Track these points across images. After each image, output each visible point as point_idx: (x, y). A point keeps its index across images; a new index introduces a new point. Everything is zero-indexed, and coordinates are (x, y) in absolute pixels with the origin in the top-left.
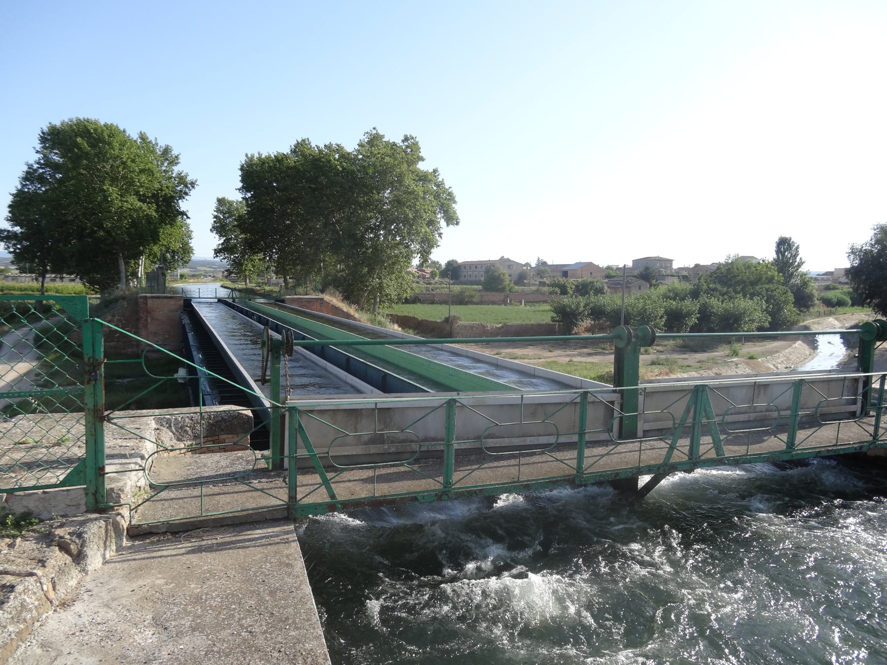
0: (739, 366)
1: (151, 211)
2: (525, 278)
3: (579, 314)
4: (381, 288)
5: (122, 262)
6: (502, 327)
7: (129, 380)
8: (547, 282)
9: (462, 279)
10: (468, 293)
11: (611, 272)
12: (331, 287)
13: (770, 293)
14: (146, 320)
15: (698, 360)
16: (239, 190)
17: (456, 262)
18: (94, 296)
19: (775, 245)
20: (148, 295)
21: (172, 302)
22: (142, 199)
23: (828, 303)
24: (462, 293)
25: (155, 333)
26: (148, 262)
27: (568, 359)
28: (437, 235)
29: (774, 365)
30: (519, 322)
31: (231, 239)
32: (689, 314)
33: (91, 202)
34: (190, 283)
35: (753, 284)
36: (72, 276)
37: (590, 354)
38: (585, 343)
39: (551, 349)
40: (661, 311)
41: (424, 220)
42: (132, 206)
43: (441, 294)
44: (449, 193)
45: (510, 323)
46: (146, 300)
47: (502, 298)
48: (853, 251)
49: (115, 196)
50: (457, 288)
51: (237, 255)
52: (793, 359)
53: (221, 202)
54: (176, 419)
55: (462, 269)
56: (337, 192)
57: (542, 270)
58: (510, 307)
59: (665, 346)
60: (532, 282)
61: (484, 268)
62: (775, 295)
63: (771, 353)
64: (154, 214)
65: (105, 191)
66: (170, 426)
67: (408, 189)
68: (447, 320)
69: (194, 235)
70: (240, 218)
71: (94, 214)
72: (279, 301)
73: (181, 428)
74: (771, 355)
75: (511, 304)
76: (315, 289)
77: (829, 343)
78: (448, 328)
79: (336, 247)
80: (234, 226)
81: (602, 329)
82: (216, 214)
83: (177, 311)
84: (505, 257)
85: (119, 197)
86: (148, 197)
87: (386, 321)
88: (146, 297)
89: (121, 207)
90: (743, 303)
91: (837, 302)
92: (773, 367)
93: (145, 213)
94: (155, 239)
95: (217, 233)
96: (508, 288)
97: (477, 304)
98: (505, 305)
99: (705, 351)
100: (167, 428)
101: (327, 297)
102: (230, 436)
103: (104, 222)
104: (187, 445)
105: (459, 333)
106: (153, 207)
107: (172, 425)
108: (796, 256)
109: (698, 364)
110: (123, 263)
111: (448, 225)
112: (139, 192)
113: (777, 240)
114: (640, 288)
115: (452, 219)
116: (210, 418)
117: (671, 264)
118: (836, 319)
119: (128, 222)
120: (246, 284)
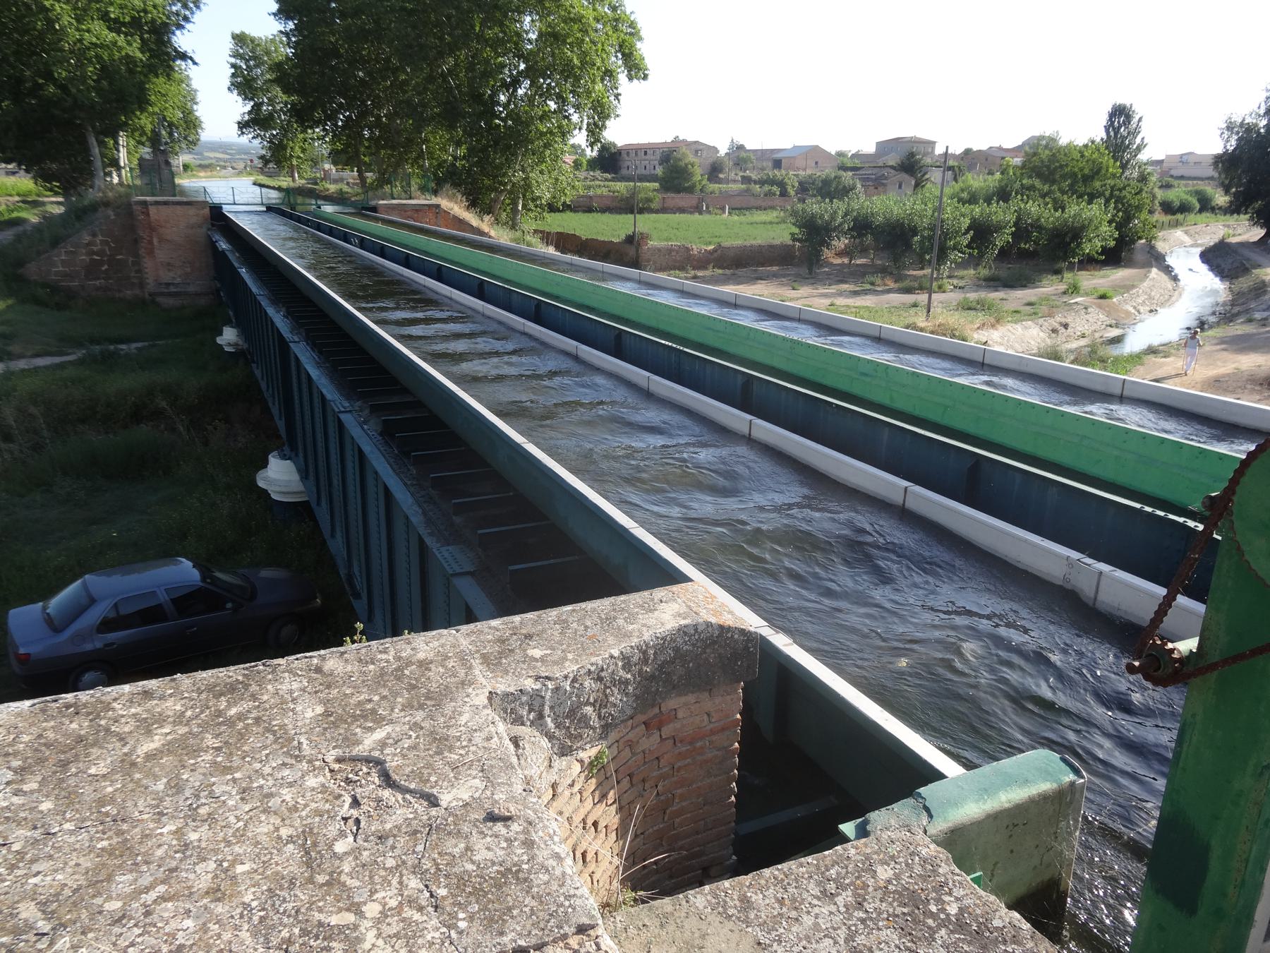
0: (1089, 310)
1: (133, 49)
2: (721, 171)
3: (835, 229)
4: (527, 186)
5: (92, 141)
6: (715, 251)
7: (139, 345)
8: (754, 177)
9: (624, 172)
10: (642, 195)
11: (845, 160)
12: (448, 186)
13: (1117, 193)
14: (151, 242)
15: (1025, 301)
16: (275, 15)
17: (614, 145)
18: (54, 199)
19: (1106, 117)
20: (148, 198)
21: (192, 211)
22: (115, 25)
23: (1168, 208)
24: (633, 193)
25: (169, 264)
26: (132, 142)
27: (827, 301)
28: (612, 98)
29: (1135, 308)
30: (738, 242)
31: (262, 104)
32: (999, 228)
33: (27, 32)
34: (201, 177)
35: (1087, 179)
36: (10, 166)
37: (856, 293)
38: (841, 276)
39: (795, 285)
40: (966, 222)
41: (598, 69)
42: (98, 39)
43: (601, 196)
44: (632, 22)
45: (727, 243)
46: (147, 209)
47: (694, 202)
48: (1230, 127)
49: (66, 20)
50: (621, 187)
51: (274, 132)
52: (1156, 298)
53: (240, 39)
54: (557, 689)
55: (624, 155)
56: (449, 17)
57: (743, 158)
58: (706, 217)
59: (962, 278)
60: (732, 175)
61: (658, 153)
62: (1125, 197)
63: (1126, 288)
64: (139, 55)
65: (47, 10)
66: (541, 716)
67: (569, 13)
68: (630, 239)
69: (199, 97)
70: (278, 67)
71: (34, 53)
72: (366, 210)
73: (572, 713)
74: (1128, 292)
75: (709, 212)
76: (423, 189)
77: (1191, 270)
78: (631, 251)
79: (450, 116)
80: (267, 81)
81: (864, 251)
82: (233, 60)
83: (200, 226)
84: (681, 138)
85: (74, 21)
86: (124, 24)
87: (535, 240)
88: (145, 203)
89: (80, 41)
90: (1076, 210)
91: (1180, 207)
92: (1133, 311)
93: (123, 54)
94: (142, 102)
95: (239, 94)
96: (699, 187)
97: (657, 212)
98: (701, 213)
99: (1024, 286)
100: (532, 724)
101: (445, 203)
102: (691, 698)
103: (54, 68)
104: (587, 761)
105: (649, 261)
106: (135, 41)
107: (547, 711)
108: (1136, 132)
109: (1028, 308)
110: (95, 143)
111: (630, 78)
112: (107, 13)
113: (1108, 108)
114: (900, 187)
115: (636, 69)
116: (645, 661)
117: (933, 149)
118: (1186, 232)
119: (95, 68)
120: (294, 180)
